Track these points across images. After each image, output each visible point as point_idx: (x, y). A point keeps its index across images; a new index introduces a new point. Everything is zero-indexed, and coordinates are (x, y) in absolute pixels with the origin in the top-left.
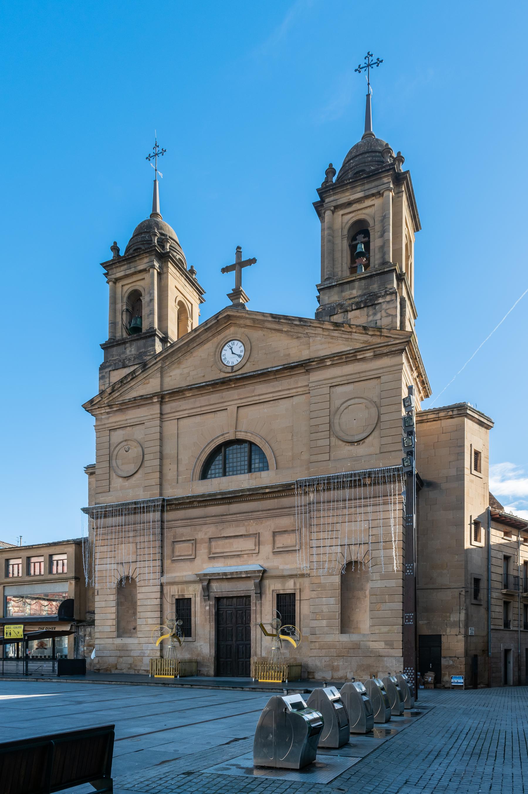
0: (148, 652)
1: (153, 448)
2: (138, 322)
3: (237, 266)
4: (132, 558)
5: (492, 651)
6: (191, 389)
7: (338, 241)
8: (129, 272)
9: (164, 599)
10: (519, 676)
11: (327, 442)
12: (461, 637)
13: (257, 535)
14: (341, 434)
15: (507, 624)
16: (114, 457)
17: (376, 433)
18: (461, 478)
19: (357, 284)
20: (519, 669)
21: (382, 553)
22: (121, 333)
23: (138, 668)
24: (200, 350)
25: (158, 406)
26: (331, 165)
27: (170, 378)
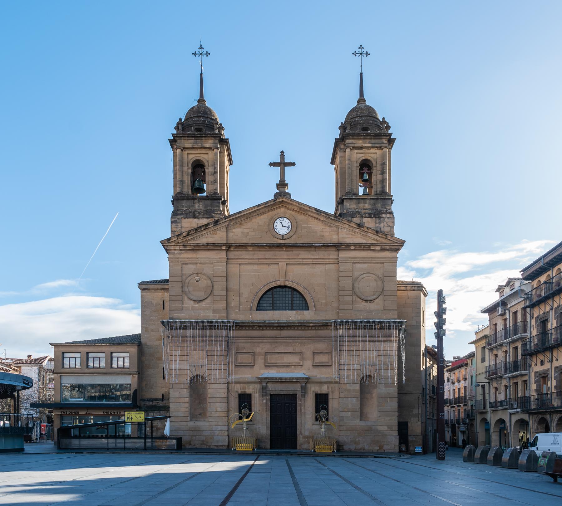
1: (220, 283)
8: (195, 146)
11: (350, 298)
14: (359, 294)
16: (186, 285)
17: (381, 297)
19: (368, 201)
22: (187, 190)
24: (258, 218)
25: (225, 253)
27: (233, 234)
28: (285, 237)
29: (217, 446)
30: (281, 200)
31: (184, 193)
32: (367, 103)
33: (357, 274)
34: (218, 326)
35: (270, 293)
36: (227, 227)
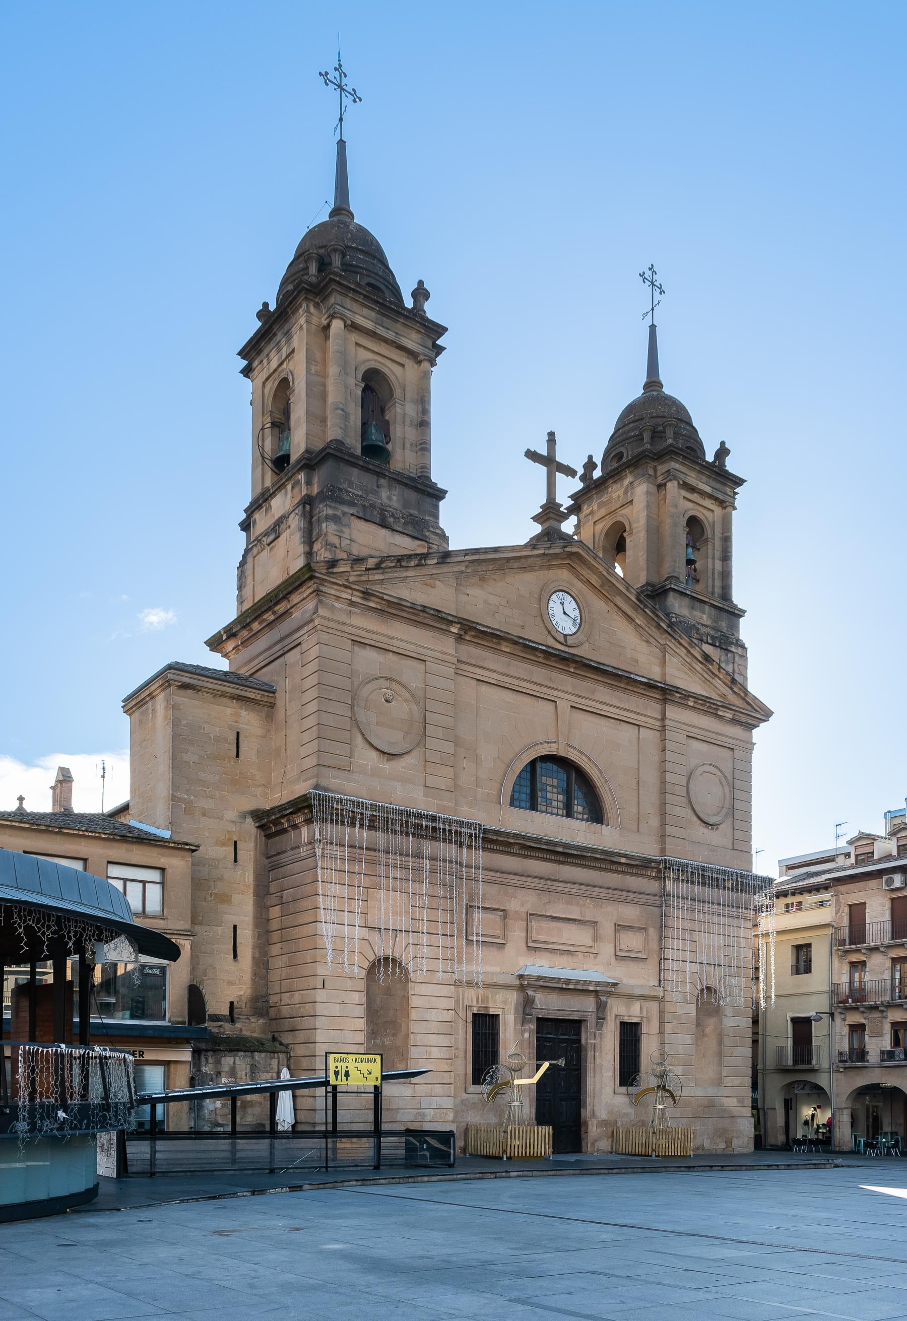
4: (403, 923)
6: (516, 643)
8: (381, 331)
26: (421, 283)
27: (466, 598)
32: (667, 390)
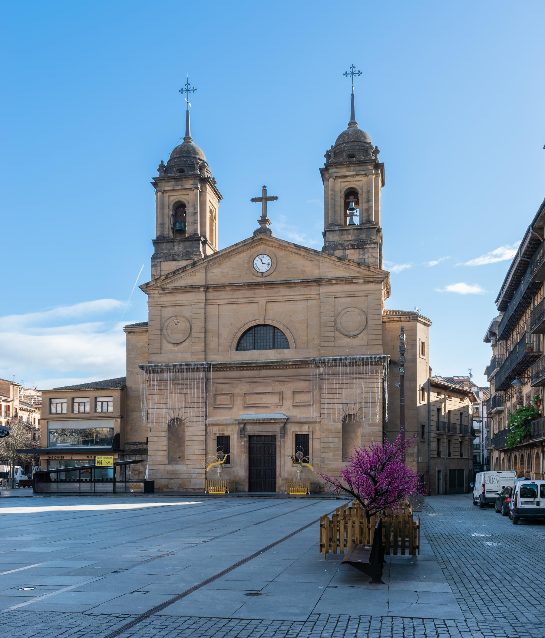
0: (194, 475)
1: (199, 324)
2: (183, 226)
3: (264, 200)
5: (431, 472)
7: (338, 199)
8: (176, 188)
9: (207, 436)
10: (446, 488)
11: (332, 334)
12: (415, 463)
13: (281, 393)
14: (342, 330)
15: (439, 454)
16: (165, 328)
17: (365, 332)
18: (414, 361)
19: (351, 232)
20: (446, 484)
21: (370, 409)
22: (168, 232)
23: (186, 487)
24: (237, 257)
25: (203, 294)
28: (265, 275)
29: (195, 489)
30: (259, 237)
31: (165, 235)
32: (359, 127)
33: (339, 309)
34: (194, 368)
35: (251, 332)
36: (206, 268)
